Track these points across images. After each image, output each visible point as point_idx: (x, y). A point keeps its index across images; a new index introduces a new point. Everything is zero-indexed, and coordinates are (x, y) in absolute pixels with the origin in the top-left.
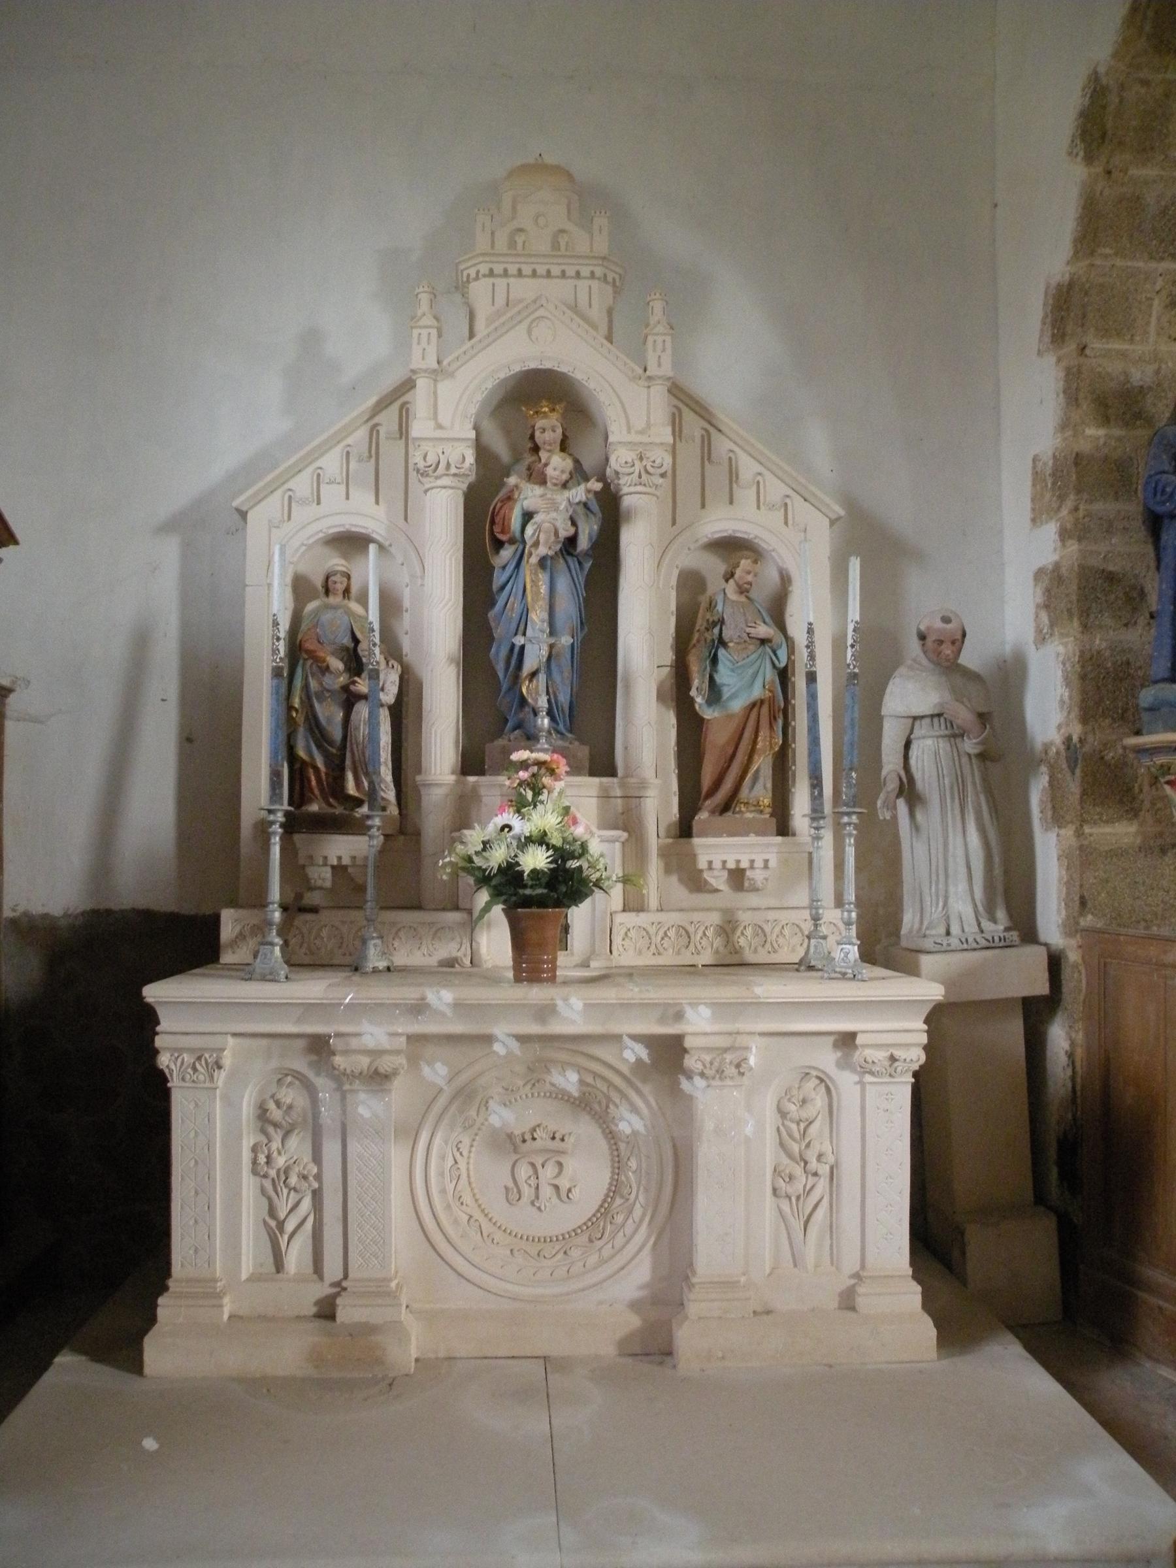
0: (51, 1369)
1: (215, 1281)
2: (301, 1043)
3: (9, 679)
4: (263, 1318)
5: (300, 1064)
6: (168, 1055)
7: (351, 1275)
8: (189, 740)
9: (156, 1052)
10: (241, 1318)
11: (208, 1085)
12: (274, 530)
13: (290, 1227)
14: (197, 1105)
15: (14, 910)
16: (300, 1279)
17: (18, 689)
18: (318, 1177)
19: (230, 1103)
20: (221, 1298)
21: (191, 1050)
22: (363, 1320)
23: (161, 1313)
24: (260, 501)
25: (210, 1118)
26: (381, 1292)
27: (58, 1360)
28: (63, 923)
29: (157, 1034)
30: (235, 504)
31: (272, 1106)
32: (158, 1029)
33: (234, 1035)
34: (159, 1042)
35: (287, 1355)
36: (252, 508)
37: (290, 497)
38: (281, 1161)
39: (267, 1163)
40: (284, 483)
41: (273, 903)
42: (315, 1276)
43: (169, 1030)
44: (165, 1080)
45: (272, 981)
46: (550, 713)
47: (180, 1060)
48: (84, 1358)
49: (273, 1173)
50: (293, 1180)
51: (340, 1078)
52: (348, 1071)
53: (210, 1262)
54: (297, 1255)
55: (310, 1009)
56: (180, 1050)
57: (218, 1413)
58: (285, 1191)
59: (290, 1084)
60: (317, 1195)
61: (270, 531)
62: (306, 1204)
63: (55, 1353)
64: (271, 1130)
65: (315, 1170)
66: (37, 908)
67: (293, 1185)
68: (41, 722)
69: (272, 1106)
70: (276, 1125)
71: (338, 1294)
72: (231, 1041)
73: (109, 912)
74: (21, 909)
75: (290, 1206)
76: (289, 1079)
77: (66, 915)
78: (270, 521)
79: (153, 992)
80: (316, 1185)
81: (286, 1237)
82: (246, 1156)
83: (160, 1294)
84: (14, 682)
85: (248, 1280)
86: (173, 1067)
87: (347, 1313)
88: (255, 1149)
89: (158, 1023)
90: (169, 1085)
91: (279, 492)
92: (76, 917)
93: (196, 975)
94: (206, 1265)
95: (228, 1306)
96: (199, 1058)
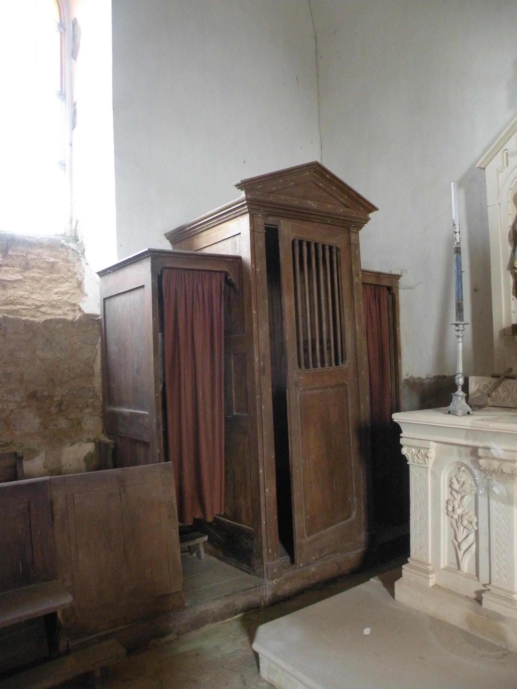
0: (367, 583)
1: (428, 564)
2: (469, 450)
3: (400, 271)
4: (450, 592)
5: (467, 461)
6: (406, 448)
7: (493, 583)
8: (476, 290)
9: (401, 446)
10: (440, 587)
11: (424, 465)
12: (499, 173)
13: (464, 547)
14: (420, 475)
15: (407, 376)
16: (467, 576)
17: (403, 275)
18: (477, 524)
19: (436, 477)
20: (429, 574)
21: (415, 447)
22: (496, 610)
23: (403, 572)
24: (491, 160)
25: (426, 481)
26: (507, 597)
27: (372, 580)
28: (426, 381)
29: (401, 437)
30: (477, 165)
31: (455, 481)
32: (401, 435)
33: (436, 442)
34: (402, 441)
35: (456, 614)
36: (487, 165)
37: (507, 153)
38: (459, 511)
39: (453, 511)
40: (502, 147)
41: (458, 374)
42: (476, 578)
43: (407, 436)
44: (406, 461)
45: (455, 415)
46: (5, 322)
47: (411, 451)
48: (380, 583)
49: (456, 516)
50: (465, 523)
51: (487, 472)
52: (487, 468)
53: (427, 554)
54: (467, 563)
55: (470, 432)
56: (412, 447)
57: (408, 627)
58: (462, 528)
59: (464, 471)
60: (477, 532)
61: (498, 175)
62: (472, 537)
63: (372, 576)
64: (454, 493)
65: (475, 520)
66: (416, 375)
67: (465, 525)
68: (413, 289)
69: (455, 481)
70: (457, 492)
71: (484, 591)
72: (433, 445)
73: (444, 377)
74: (410, 375)
75: (464, 536)
76: (463, 468)
77: (427, 378)
78: (497, 170)
79: (397, 417)
80: (476, 528)
81: (462, 552)
82: (443, 505)
83: (404, 564)
84: (401, 272)
85: (444, 569)
86: (408, 454)
87: (488, 602)
88: (447, 502)
89: (401, 432)
90: (408, 463)
91: (500, 154)
92: (431, 379)
93: (484, 411)
94: (424, 556)
95: (432, 580)
96: (419, 452)
